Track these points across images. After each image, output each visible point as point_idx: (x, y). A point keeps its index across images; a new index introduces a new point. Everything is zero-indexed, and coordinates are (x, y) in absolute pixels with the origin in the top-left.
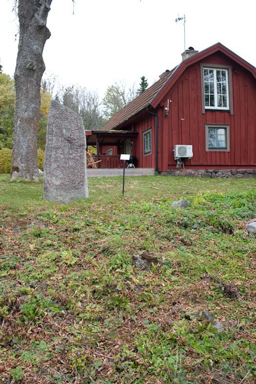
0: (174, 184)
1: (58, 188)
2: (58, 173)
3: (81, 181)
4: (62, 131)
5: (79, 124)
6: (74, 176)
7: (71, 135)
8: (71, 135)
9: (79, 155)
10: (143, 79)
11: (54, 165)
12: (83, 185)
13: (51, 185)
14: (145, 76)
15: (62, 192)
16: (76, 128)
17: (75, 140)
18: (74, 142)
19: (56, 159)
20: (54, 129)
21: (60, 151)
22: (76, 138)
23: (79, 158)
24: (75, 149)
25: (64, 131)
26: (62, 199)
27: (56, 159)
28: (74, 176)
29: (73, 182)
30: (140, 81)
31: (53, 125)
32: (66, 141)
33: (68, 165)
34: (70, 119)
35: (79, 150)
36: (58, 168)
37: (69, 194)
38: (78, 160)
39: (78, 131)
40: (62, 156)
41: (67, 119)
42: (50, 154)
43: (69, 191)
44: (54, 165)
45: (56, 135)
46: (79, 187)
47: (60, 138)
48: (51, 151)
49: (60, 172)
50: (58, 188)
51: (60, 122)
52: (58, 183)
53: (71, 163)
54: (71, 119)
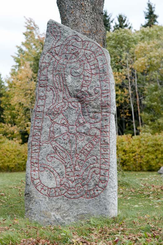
0: (69, 218)
1: (51, 194)
2: (55, 163)
3: (100, 180)
4: (64, 80)
5: (100, 64)
6: (86, 170)
7: (82, 86)
8: (82, 86)
9: (98, 125)
10: (149, 5)
11: (47, 148)
12: (104, 188)
13: (39, 188)
14: (22, 41)
15: (60, 202)
16: (94, 72)
17: (90, 95)
18: (88, 99)
19: (52, 135)
20: (50, 77)
21: (59, 119)
22: (91, 91)
23: (98, 133)
24: (91, 115)
25: (69, 79)
26: (58, 217)
27: (52, 135)
28: (86, 170)
29: (83, 181)
30: (144, 13)
31: (49, 69)
32: (74, 99)
33: (74, 146)
34: (81, 54)
35: (99, 116)
36: (55, 153)
37: (75, 207)
38: (95, 136)
39: (98, 76)
40: (64, 129)
41: (76, 54)
42: (40, 125)
43: (76, 201)
44: (47, 148)
45: (54, 88)
46: (97, 193)
47: (60, 94)
48: (42, 120)
49: (58, 162)
50: (51, 194)
51: (61, 61)
52: (52, 184)
53: (82, 143)
54: (84, 55)
